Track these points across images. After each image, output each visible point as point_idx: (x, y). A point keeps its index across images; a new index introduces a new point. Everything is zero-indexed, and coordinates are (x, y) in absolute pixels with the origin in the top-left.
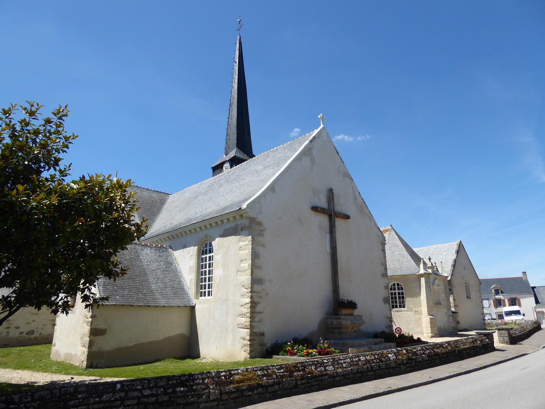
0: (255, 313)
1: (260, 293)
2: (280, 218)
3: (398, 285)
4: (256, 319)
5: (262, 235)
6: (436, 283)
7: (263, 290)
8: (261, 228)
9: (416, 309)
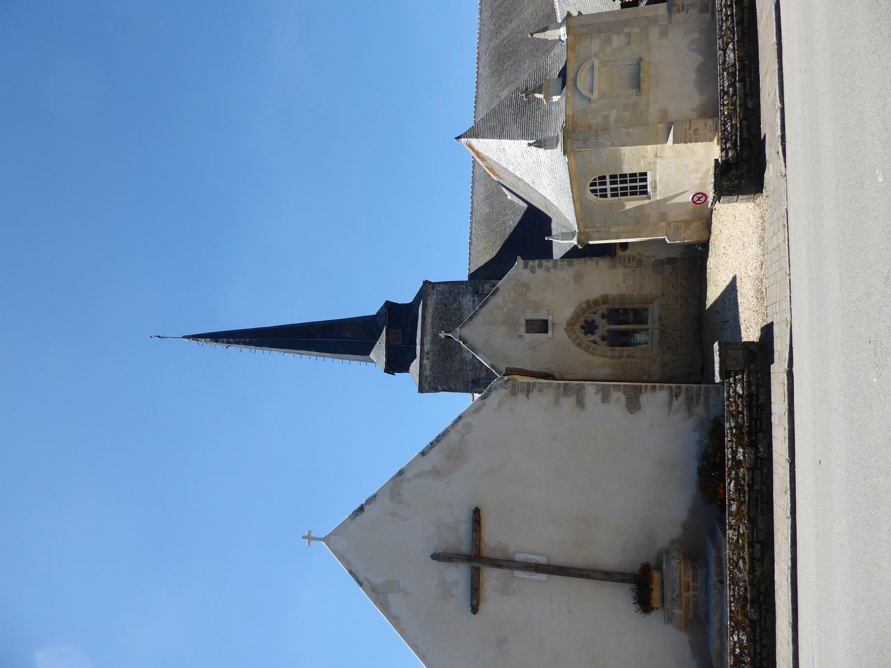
3: (592, 184)
6: (586, 93)
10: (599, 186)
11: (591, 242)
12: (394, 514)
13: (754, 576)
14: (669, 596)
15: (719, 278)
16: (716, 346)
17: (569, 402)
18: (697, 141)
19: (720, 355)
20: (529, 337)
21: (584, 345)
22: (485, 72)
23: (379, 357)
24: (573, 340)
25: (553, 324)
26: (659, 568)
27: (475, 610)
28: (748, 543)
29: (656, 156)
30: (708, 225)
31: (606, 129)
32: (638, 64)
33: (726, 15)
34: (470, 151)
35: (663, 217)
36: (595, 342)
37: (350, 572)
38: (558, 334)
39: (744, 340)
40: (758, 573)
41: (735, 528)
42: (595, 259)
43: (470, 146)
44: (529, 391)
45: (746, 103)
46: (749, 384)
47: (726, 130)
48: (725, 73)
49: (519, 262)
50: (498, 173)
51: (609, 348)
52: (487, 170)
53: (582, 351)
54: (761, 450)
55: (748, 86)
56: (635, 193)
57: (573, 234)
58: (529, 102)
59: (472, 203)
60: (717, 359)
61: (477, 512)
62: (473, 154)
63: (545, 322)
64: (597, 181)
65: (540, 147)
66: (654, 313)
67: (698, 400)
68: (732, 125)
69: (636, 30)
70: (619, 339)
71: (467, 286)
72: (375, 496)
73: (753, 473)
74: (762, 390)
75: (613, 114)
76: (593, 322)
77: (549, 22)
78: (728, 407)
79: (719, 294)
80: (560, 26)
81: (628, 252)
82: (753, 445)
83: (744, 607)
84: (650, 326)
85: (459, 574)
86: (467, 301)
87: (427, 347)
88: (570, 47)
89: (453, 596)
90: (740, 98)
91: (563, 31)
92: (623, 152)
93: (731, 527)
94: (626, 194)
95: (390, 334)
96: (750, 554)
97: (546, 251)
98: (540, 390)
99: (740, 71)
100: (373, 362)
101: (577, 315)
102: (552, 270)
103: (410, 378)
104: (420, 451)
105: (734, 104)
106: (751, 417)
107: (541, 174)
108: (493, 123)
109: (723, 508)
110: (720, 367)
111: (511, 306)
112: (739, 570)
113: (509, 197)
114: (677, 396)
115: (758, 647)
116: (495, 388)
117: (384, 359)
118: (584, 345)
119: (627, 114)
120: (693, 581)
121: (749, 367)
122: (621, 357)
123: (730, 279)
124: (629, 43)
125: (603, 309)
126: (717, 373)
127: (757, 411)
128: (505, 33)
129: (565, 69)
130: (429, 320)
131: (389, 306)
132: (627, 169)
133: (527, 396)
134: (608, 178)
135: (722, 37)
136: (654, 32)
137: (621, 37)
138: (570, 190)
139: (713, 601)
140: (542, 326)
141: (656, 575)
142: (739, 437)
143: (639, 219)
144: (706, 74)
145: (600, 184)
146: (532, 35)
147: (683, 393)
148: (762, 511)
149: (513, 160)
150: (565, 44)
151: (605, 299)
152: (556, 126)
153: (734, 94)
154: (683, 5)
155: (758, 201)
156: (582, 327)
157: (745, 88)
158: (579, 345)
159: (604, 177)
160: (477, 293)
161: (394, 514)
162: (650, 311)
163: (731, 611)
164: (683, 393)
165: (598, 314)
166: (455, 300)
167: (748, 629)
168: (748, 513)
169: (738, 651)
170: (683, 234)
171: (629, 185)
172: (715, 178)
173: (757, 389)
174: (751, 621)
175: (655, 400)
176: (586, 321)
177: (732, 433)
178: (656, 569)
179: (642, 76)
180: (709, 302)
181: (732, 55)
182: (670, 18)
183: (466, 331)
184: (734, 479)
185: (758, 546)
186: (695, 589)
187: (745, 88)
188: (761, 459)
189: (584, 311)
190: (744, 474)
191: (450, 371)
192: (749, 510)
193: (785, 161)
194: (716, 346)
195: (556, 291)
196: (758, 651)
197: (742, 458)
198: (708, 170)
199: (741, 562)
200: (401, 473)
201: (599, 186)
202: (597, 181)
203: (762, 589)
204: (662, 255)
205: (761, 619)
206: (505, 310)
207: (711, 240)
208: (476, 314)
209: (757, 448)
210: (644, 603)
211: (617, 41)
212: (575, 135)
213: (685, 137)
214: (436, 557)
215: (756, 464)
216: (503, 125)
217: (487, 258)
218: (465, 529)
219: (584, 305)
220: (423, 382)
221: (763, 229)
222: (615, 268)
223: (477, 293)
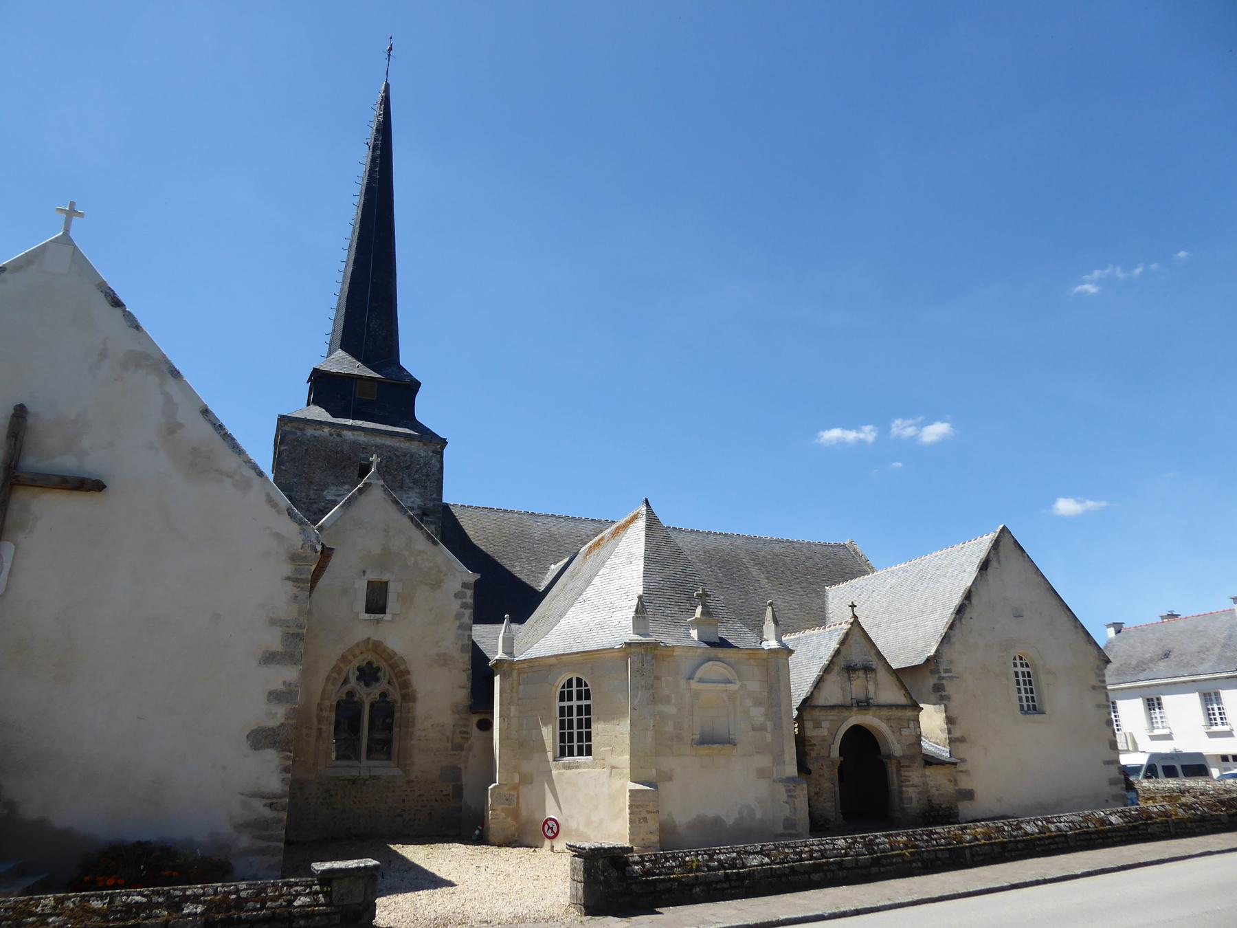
3: (579, 681)
6: (698, 674)
10: (577, 690)
11: (497, 679)
12: (103, 354)
15: (440, 861)
16: (371, 862)
17: (274, 640)
18: (631, 822)
19: (358, 869)
20: (361, 586)
21: (342, 665)
22: (710, 543)
23: (338, 362)
24: (351, 650)
25: (378, 621)
29: (613, 767)
30: (511, 842)
31: (654, 700)
32: (729, 742)
33: (802, 852)
34: (628, 518)
35: (526, 779)
36: (346, 681)
38: (363, 628)
39: (378, 901)
41: (57, 909)
42: (469, 684)
43: (635, 518)
46: (312, 915)
47: (667, 860)
48: (734, 855)
49: (472, 577)
50: (595, 552)
51: (335, 703)
52: (597, 539)
53: (334, 663)
56: (562, 739)
57: (511, 654)
58: (690, 598)
59: (546, 516)
60: (352, 864)
62: (623, 521)
63: (383, 610)
65: (637, 611)
66: (385, 769)
67: (261, 838)
68: (673, 867)
69: (769, 737)
70: (347, 715)
71: (434, 500)
72: (137, 327)
75: (671, 710)
76: (377, 680)
77: (782, 628)
78: (273, 885)
79: (417, 862)
80: (779, 641)
81: (475, 730)
84: (364, 762)
86: (413, 499)
87: (348, 435)
88: (755, 652)
91: (772, 644)
92: (622, 723)
94: (562, 727)
95: (369, 382)
97: (486, 612)
98: (296, 597)
100: (330, 353)
101: (389, 656)
102: (457, 623)
103: (297, 403)
104: (211, 408)
105: (698, 869)
107: (596, 608)
108: (665, 550)
109: (76, 886)
110: (340, 870)
111: (411, 561)
113: (553, 567)
114: (271, 805)
116: (303, 530)
117: (334, 369)
118: (342, 665)
119: (669, 728)
121: (336, 913)
122: (320, 720)
123: (448, 878)
124: (754, 729)
125: (395, 695)
126: (328, 865)
128: (754, 571)
129: (730, 646)
130: (388, 442)
131: (415, 386)
132: (597, 728)
133: (288, 578)
134: (588, 702)
135: (776, 848)
136: (764, 761)
137: (762, 719)
138: (575, 650)
140: (376, 602)
142: (222, 904)
143: (523, 745)
144: (712, 832)
145: (579, 692)
146: (770, 604)
147: (275, 814)
149: (615, 575)
150: (758, 646)
151: (409, 697)
152: (661, 635)
153: (710, 869)
154: (794, 797)
155: (572, 910)
156: (370, 663)
157: (717, 883)
158: (344, 658)
159: (588, 698)
160: (424, 514)
161: (103, 354)
162: (386, 763)
164: (275, 814)
165: (387, 686)
166: (415, 482)
172: (609, 849)
175: (267, 772)
176: (378, 669)
177: (230, 893)
179: (715, 746)
180: (397, 848)
181: (755, 862)
183: (377, 495)
184: (150, 901)
187: (717, 883)
189: (393, 666)
190: (157, 917)
191: (306, 467)
194: (371, 862)
195: (426, 629)
197: (186, 911)
198: (588, 840)
200: (176, 374)
201: (577, 690)
204: (467, 779)
206: (406, 553)
207: (493, 848)
208: (403, 510)
211: (758, 714)
213: (637, 806)
214: (20, 413)
216: (662, 563)
217: (470, 532)
218: (68, 464)
219: (403, 667)
220: (295, 424)
221: (536, 921)
222: (454, 712)
223: (424, 514)
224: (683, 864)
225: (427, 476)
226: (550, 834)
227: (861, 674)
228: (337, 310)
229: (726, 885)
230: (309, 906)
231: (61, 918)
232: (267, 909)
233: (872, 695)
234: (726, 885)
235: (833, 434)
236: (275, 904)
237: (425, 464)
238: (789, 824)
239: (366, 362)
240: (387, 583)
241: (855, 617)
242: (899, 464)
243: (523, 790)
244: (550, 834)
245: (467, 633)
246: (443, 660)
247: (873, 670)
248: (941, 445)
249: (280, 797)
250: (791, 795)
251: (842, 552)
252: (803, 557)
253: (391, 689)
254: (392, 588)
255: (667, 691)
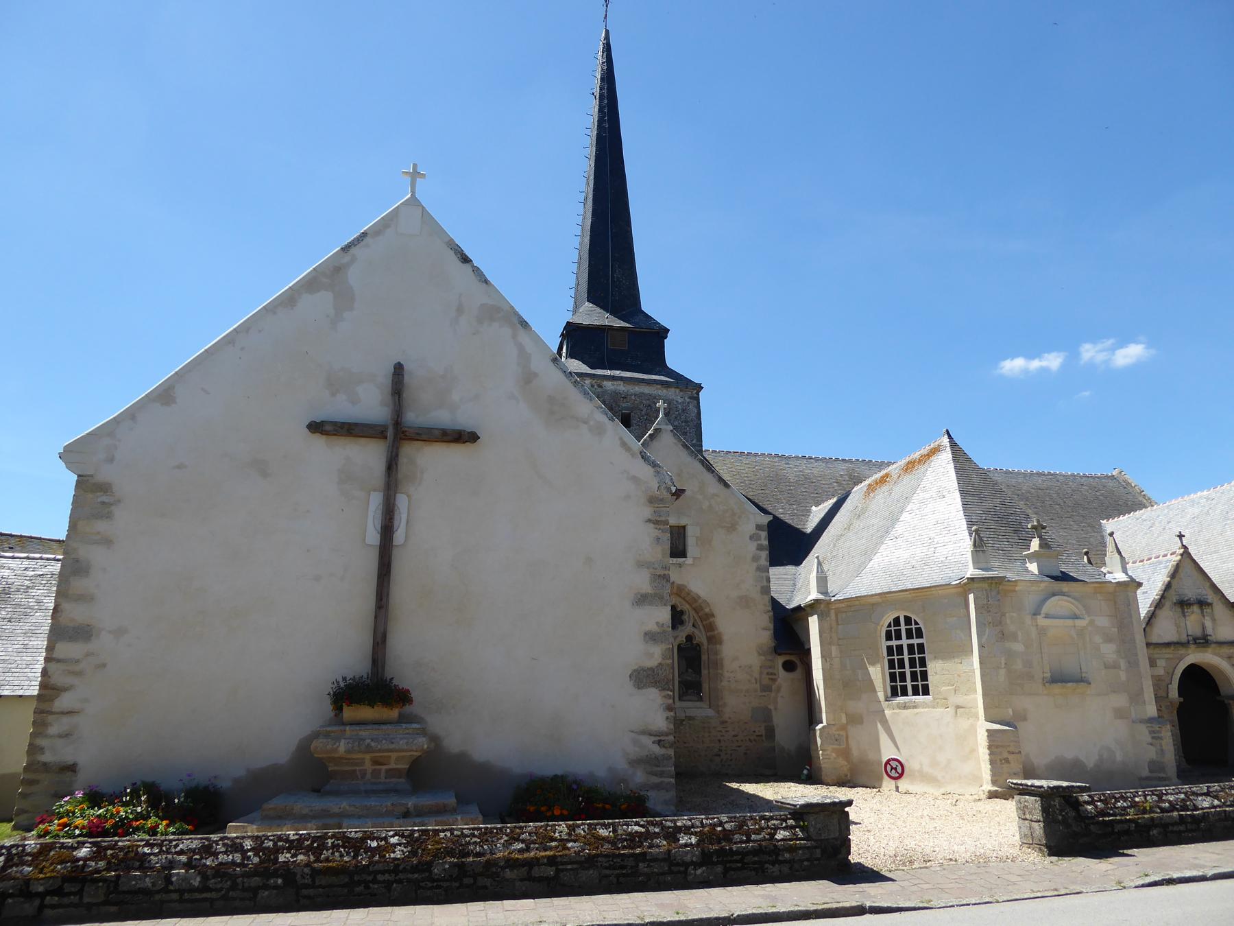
0: (50, 713)
1: (77, 661)
2: (180, 467)
3: (908, 620)
4: (53, 730)
5: (109, 516)
6: (1044, 610)
7: (88, 655)
8: (105, 499)
9: (959, 699)
13: (503, 868)
14: (365, 732)
17: (643, 583)
25: (680, 566)
26: (403, 719)
27: (316, 427)
28: (554, 857)
29: (958, 707)
32: (1081, 680)
34: (924, 451)
35: (856, 720)
37: (364, 234)
40: (508, 874)
42: (771, 626)
43: (935, 451)
44: (656, 522)
45: (1156, 826)
46: (792, 849)
47: (1117, 800)
48: (1182, 796)
54: (699, 872)
55: (1175, 828)
61: (473, 437)
63: (683, 554)
64: (913, 627)
72: (486, 281)
73: (664, 860)
74: (786, 869)
75: (1018, 647)
81: (781, 672)
82: (706, 859)
83: (449, 852)
85: (371, 404)
89: (333, 395)
90: (1161, 818)
93: (572, 829)
96: (537, 859)
99: (1192, 816)
101: (693, 600)
106: (744, 854)
112: (507, 844)
115: (387, 877)
117: (586, 321)
119: (1019, 665)
120: (388, 771)
121: (816, 847)
125: (701, 637)
127: (754, 863)
131: (663, 332)
132: (933, 667)
133: (649, 521)
134: (920, 641)
135: (1223, 790)
137: (1115, 656)
138: (902, 587)
139: (372, 802)
141: (394, 713)
143: (849, 683)
147: (663, 751)
148: (607, 876)
151: (715, 639)
153: (1163, 810)
154: (1161, 738)
161: (460, 310)
162: (698, 704)
163: (436, 832)
164: (663, 751)
165: (693, 629)
167: (415, 861)
168: (601, 855)
169: (374, 844)
170: (830, 748)
171: (908, 670)
173: (786, 861)
174: (430, 864)
177: (715, 825)
178: (400, 714)
181: (1206, 804)
182: (1141, 721)
185: (551, 872)
186: (376, 773)
187: (1173, 825)
188: (685, 873)
190: (658, 846)
192: (607, 856)
193: (1143, 886)
195: (723, 575)
196: (380, 877)
199: (521, 846)
200: (524, 324)
202: (913, 627)
203: (482, 881)
205: (434, 881)
206: (700, 497)
209: (700, 865)
210: (348, 694)
211: (1109, 651)
212: (994, 593)
213: (997, 747)
214: (399, 369)
215: (678, 864)
216: (977, 495)
218: (442, 418)
219: (707, 610)
222: (760, 654)
224: (1134, 805)
225: (686, 422)
226: (893, 774)
227: (1196, 608)
228: (579, 263)
229: (1182, 828)
230: (791, 840)
231: (577, 844)
232: (754, 841)
233: (1209, 631)
234: (1182, 828)
235: (1014, 365)
236: (759, 837)
237: (683, 410)
238: (1156, 766)
239: (615, 313)
240: (684, 527)
241: (1185, 547)
242: (1087, 394)
243: (853, 731)
244: (893, 774)
245: (764, 574)
246: (744, 602)
247: (1210, 605)
248: (1135, 370)
249: (667, 734)
250: (1156, 736)
251: (1111, 483)
252: (1069, 490)
253: (696, 632)
254: (690, 532)
255: (1012, 628)
